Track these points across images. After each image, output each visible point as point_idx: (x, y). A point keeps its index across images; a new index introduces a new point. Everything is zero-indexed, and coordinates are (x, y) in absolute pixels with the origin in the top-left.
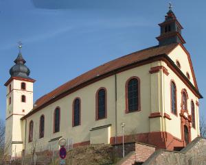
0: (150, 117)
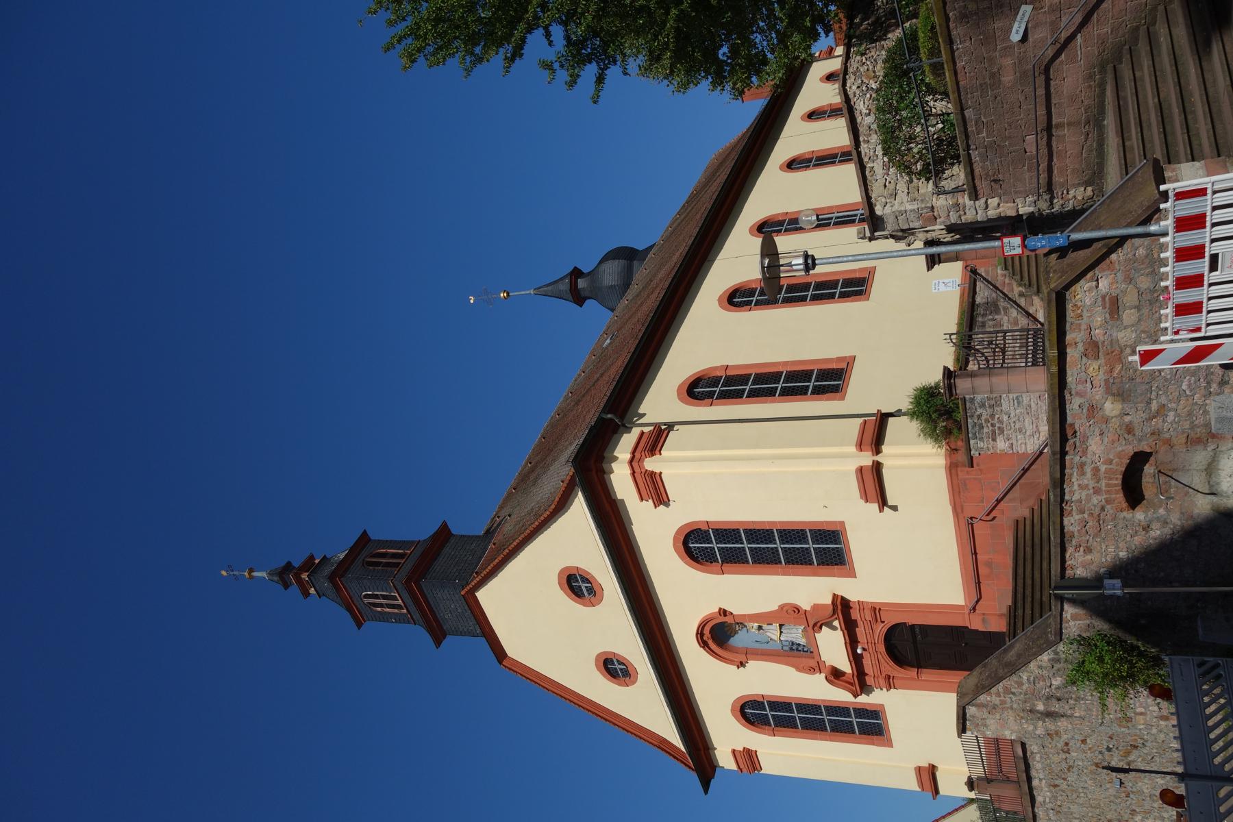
0: (883, 502)
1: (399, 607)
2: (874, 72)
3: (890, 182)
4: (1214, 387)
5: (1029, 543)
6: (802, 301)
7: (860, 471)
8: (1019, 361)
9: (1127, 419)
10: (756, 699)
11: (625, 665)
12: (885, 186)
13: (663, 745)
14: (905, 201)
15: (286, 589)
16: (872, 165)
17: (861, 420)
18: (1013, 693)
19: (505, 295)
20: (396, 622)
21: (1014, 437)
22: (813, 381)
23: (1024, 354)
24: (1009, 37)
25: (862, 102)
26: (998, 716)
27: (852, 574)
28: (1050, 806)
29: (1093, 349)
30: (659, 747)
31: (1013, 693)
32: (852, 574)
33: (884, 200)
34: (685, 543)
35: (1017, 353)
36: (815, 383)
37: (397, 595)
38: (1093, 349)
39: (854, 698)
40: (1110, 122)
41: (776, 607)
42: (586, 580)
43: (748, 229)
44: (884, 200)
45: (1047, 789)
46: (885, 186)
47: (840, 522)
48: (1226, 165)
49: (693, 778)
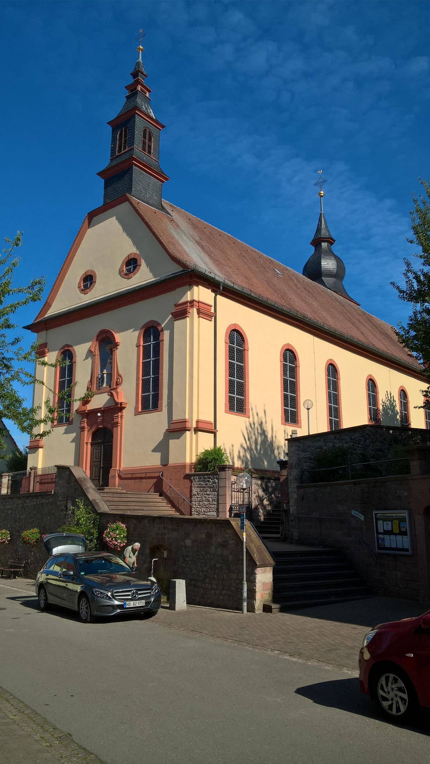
1: (120, 150)
2: (376, 442)
3: (311, 449)
4: (193, 582)
5: (149, 500)
6: (284, 389)
7: (185, 421)
8: (235, 500)
9: (184, 548)
10: (74, 358)
11: (90, 286)
12: (309, 447)
13: (47, 306)
14: (300, 456)
15: (125, 87)
16: (322, 440)
17: (213, 421)
18: (75, 492)
19: (322, 195)
20: (111, 147)
21: (198, 496)
22: (237, 396)
23: (239, 503)
24: (354, 510)
25: (358, 436)
26: (65, 484)
27: (137, 413)
28: (25, 505)
29: (209, 536)
30: (46, 303)
31: (75, 492)
32: (137, 413)
33: (301, 446)
34: (153, 327)
35: (240, 499)
36: (236, 398)
37: (127, 149)
38: (209, 536)
39: (75, 410)
40: (320, 549)
41: (177, 289)
42: (135, 268)
43: (332, 358)
44: (301, 446)
45: (32, 504)
46: (309, 447)
47: (162, 409)
48: (269, 590)
49: (31, 322)
